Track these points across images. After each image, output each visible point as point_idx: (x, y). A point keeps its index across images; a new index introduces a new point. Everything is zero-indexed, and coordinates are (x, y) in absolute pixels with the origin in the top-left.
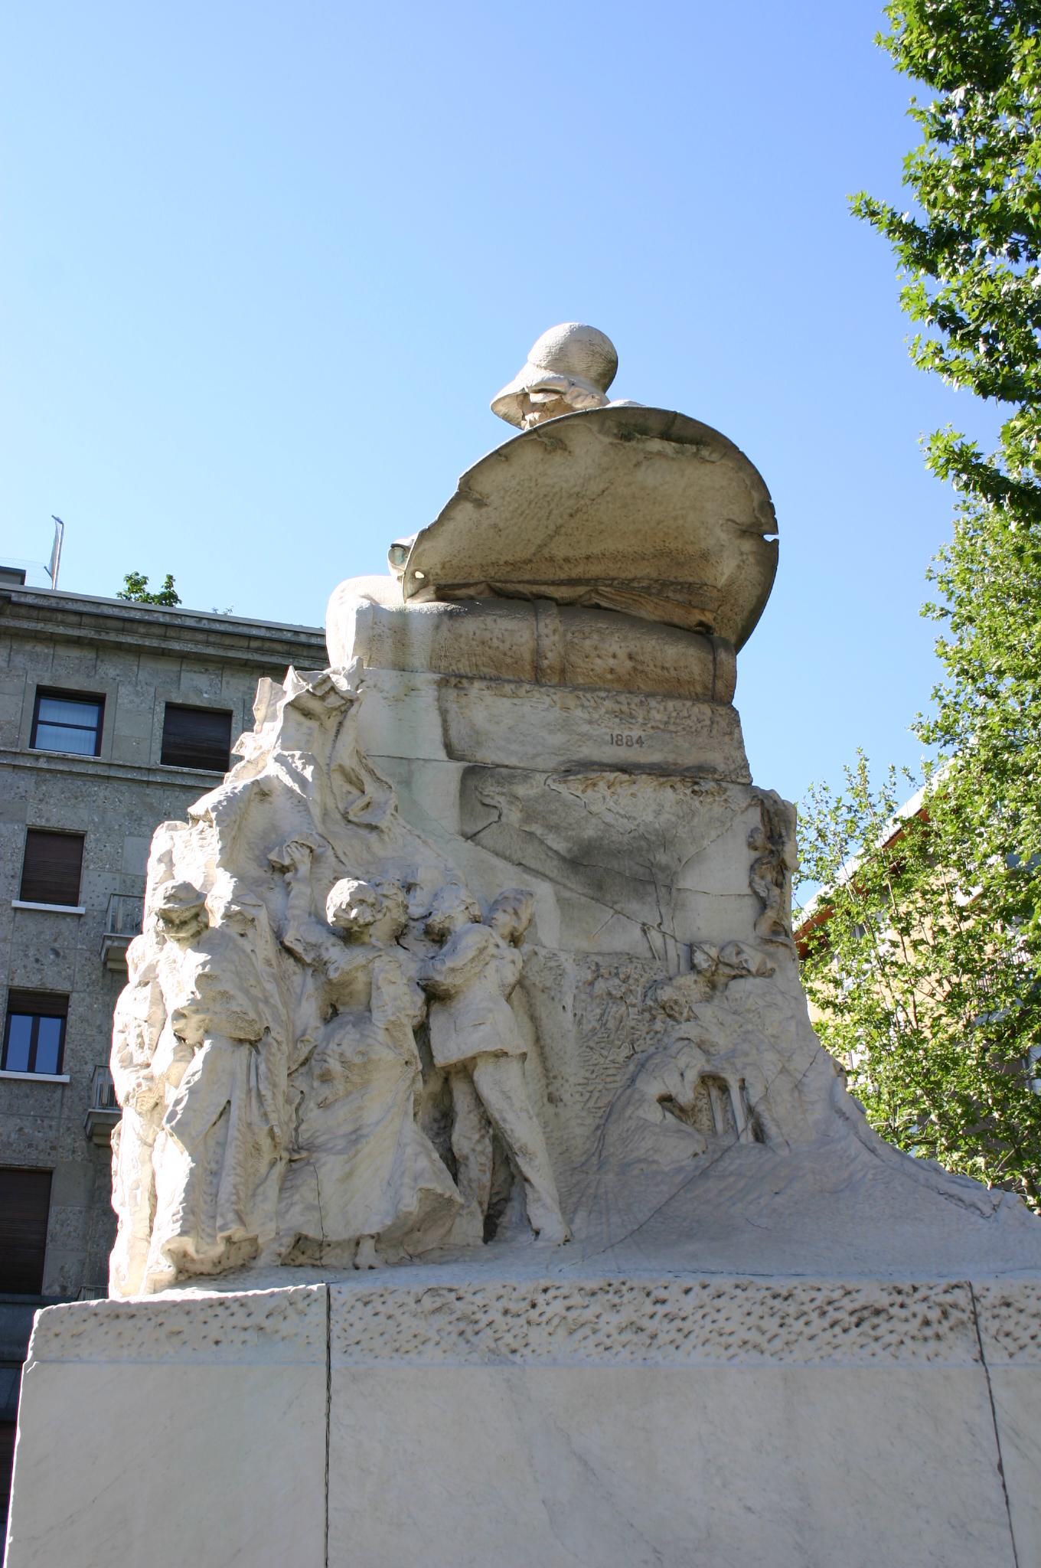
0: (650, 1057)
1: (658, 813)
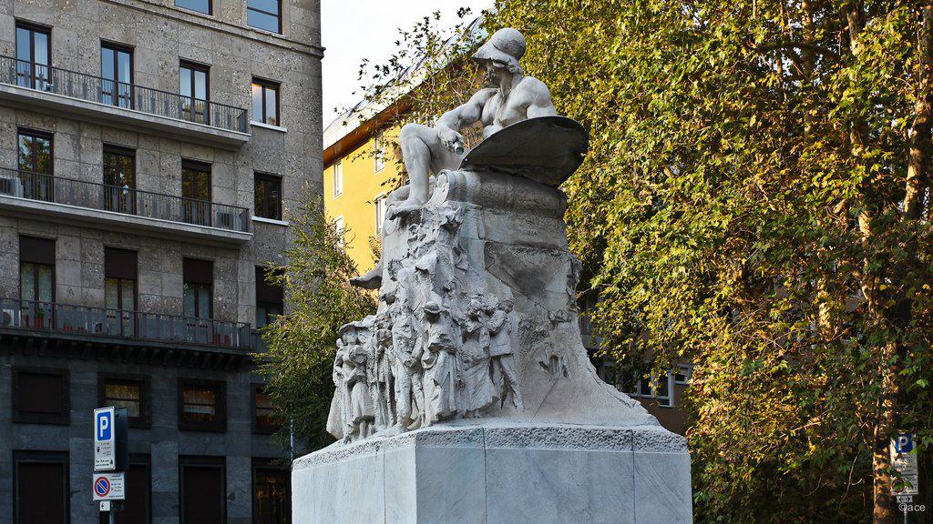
0: (511, 245)
1: (540, 262)
